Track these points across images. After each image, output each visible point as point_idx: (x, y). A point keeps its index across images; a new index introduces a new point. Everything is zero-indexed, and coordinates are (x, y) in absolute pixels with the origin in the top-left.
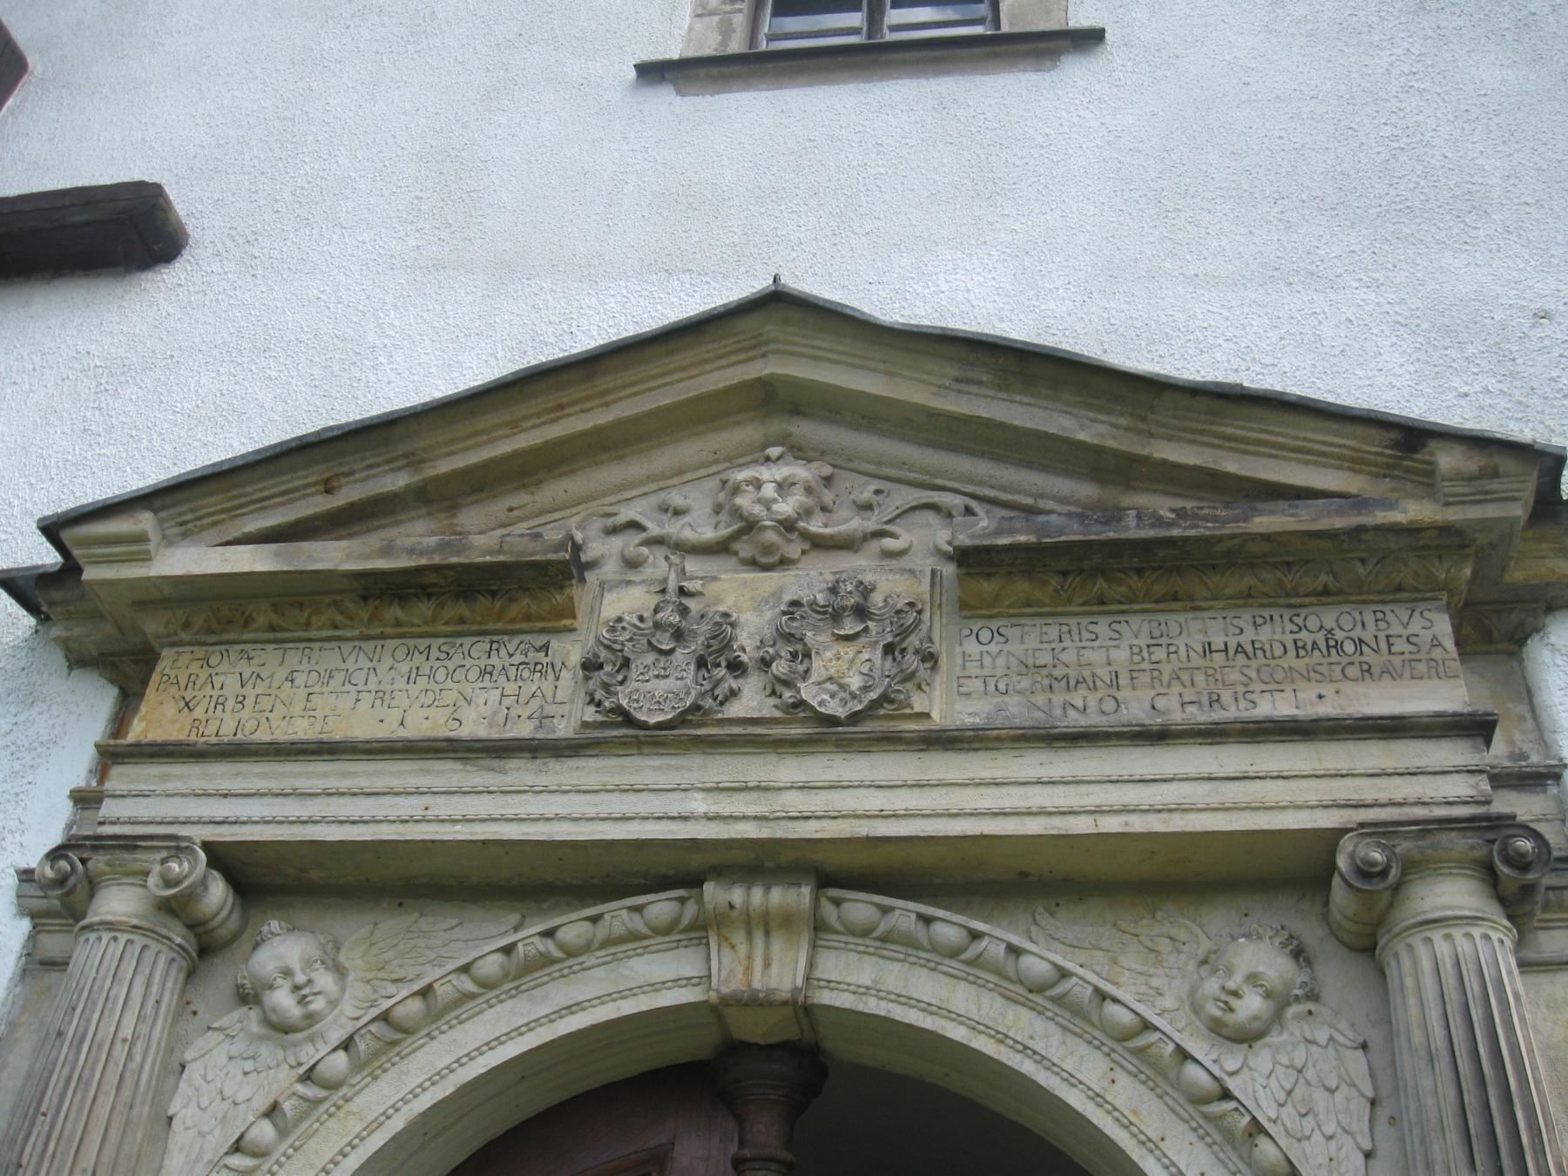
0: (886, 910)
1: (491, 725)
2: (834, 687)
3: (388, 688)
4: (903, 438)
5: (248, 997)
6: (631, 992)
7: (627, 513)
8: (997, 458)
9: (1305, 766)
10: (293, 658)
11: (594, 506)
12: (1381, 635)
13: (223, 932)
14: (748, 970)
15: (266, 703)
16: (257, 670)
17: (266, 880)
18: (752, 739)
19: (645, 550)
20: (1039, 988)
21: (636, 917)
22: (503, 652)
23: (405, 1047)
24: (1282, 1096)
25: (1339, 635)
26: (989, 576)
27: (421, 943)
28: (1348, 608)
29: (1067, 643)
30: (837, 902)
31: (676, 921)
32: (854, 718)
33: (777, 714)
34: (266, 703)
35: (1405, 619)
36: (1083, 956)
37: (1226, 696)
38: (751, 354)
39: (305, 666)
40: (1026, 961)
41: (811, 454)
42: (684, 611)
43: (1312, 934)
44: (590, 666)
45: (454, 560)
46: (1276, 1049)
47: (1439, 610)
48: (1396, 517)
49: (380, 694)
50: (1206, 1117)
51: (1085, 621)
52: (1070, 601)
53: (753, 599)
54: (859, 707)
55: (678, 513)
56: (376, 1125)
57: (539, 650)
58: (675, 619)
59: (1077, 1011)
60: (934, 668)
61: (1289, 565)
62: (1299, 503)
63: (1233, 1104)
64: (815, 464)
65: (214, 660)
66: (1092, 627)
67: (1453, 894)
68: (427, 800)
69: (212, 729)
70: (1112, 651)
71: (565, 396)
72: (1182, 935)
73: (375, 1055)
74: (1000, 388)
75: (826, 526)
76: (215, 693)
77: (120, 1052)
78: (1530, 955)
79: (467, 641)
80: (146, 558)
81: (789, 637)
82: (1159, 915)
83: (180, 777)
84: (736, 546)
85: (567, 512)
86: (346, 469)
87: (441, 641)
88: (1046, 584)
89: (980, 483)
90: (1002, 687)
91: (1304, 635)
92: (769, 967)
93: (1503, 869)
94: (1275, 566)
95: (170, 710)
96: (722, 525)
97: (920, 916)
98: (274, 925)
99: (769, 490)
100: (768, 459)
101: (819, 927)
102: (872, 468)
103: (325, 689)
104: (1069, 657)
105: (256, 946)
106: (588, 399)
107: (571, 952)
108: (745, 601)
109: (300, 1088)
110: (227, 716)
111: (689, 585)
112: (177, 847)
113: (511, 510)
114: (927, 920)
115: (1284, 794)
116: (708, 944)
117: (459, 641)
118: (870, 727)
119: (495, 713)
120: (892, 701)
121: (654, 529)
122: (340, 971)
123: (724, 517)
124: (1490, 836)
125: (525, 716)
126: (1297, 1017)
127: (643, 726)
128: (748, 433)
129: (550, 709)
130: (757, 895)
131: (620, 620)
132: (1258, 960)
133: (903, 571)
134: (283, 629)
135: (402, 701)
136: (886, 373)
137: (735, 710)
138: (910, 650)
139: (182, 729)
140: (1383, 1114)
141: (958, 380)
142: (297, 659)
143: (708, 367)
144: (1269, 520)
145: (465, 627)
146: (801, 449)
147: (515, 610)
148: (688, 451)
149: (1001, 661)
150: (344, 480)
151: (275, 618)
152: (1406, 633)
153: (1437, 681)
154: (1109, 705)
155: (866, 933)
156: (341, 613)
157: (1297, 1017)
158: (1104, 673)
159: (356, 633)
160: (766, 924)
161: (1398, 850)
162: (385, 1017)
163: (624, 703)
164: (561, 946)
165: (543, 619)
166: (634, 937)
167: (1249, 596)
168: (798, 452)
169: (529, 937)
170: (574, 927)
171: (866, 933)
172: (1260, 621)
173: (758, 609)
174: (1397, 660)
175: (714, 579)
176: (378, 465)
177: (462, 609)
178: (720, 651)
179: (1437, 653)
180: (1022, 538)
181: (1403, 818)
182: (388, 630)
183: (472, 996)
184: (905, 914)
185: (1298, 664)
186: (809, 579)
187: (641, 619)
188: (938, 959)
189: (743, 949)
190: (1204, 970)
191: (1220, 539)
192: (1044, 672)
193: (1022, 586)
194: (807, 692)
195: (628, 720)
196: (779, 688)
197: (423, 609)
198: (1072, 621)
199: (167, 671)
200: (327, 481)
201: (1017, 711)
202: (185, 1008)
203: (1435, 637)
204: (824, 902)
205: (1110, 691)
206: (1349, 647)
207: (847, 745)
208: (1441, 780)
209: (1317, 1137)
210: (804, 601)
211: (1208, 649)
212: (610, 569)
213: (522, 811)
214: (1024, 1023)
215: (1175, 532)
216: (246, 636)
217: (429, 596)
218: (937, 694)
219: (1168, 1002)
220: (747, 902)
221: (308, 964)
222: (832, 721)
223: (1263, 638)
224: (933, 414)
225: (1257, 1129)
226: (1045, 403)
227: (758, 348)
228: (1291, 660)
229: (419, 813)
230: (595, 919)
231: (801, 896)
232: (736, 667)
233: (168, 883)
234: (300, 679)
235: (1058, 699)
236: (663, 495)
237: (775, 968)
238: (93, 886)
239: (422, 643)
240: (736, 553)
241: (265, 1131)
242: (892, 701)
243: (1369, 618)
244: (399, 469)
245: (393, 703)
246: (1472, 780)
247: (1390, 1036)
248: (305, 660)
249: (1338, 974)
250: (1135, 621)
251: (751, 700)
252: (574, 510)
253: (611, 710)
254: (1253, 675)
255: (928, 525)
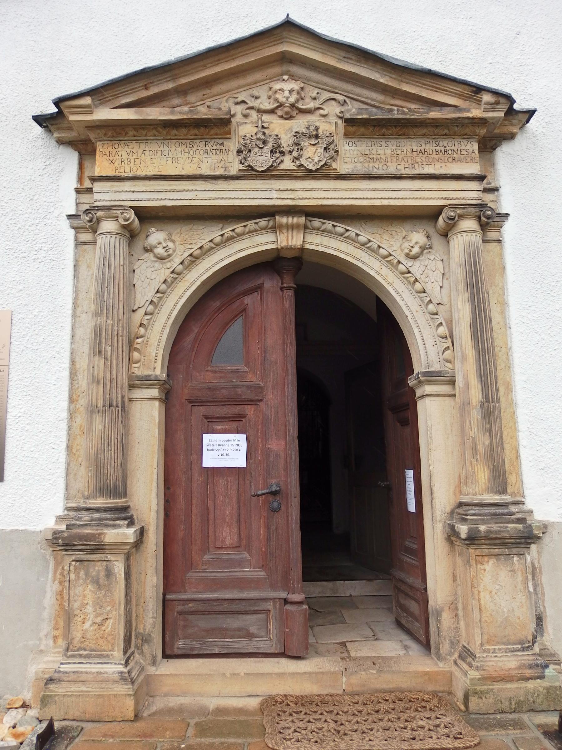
0: (323, 223)
1: (211, 170)
2: (310, 160)
3: (176, 157)
4: (325, 75)
5: (148, 250)
6: (256, 246)
7: (241, 98)
8: (354, 84)
9: (435, 187)
10: (143, 146)
11: (229, 94)
12: (459, 149)
13: (137, 232)
14: (287, 240)
15: (137, 161)
16: (132, 150)
17: (148, 216)
18: (288, 176)
19: (248, 111)
20: (364, 244)
21: (256, 225)
22: (210, 145)
23: (197, 262)
24: (422, 273)
25: (448, 148)
26: (352, 126)
27: (195, 233)
28: (451, 140)
29: (373, 147)
30: (310, 221)
31: (267, 226)
32: (317, 170)
33: (295, 168)
34: (137, 161)
35: (466, 144)
36: (373, 236)
37: (416, 165)
38: (278, 42)
39: (147, 149)
40: (360, 238)
41: (296, 78)
42: (264, 134)
43: (431, 231)
44: (239, 152)
45: (195, 117)
46: (421, 260)
47: (475, 141)
48: (470, 115)
49: (174, 159)
50: (404, 277)
51: (378, 140)
52: (375, 135)
53: (284, 130)
54: (319, 167)
55: (257, 98)
56: (192, 284)
57: (221, 145)
58: (263, 137)
59: (373, 251)
60: (337, 155)
61: (437, 126)
62: (443, 108)
63: (411, 275)
64: (298, 82)
65: (116, 146)
66: (380, 143)
67: (470, 224)
68: (196, 193)
69: (122, 170)
70: (386, 150)
71: (221, 56)
72: (399, 231)
73: (189, 265)
74: (357, 61)
75: (303, 105)
76: (120, 158)
77: (121, 268)
78: (485, 239)
79: (198, 141)
80: (91, 113)
81: (297, 144)
82: (393, 225)
83: (117, 186)
84: (277, 111)
85: (221, 96)
86: (151, 81)
87: (190, 141)
88: (369, 129)
89: (348, 92)
90: (356, 161)
91: (438, 148)
92: (292, 240)
93: (483, 219)
94: (433, 126)
95: (106, 163)
96: (271, 103)
97: (333, 225)
98: (153, 229)
99: (287, 93)
100: (284, 80)
101: (306, 227)
102: (315, 84)
103: (156, 157)
104: (374, 152)
105: (147, 236)
106: (228, 57)
107: (239, 235)
108: (282, 130)
109: (172, 275)
110: (126, 166)
111: (265, 125)
112: (124, 209)
113: (204, 95)
114: (334, 226)
115: (428, 195)
116: (276, 232)
117: (195, 141)
118: (322, 173)
119: (211, 166)
120: (327, 165)
121: (251, 104)
122: (173, 241)
123: (272, 100)
124: (481, 209)
125: (220, 167)
126: (427, 253)
127: (258, 171)
128: (276, 70)
129: (228, 165)
130: (290, 220)
131: (245, 136)
132: (417, 237)
133: (327, 122)
134: (138, 137)
135: (181, 161)
136: (322, 53)
137: (282, 166)
138: (331, 149)
139: (112, 170)
140: (445, 277)
141: (344, 57)
142: (144, 147)
143: (265, 46)
144: (435, 114)
145: (197, 137)
146: (293, 76)
147: (212, 132)
148: (258, 76)
149: (355, 152)
150: (151, 85)
151: (135, 133)
152: (466, 148)
153: (472, 164)
154: (385, 167)
155: (318, 229)
156: (157, 131)
157: (427, 253)
158: (383, 157)
159: (162, 138)
160: (292, 227)
161: (458, 212)
162: (191, 255)
163: (251, 164)
164: (236, 234)
165: (221, 135)
166: (256, 231)
167: (425, 135)
168: (293, 77)
169: (227, 231)
170: (239, 228)
171: (318, 229)
172: (426, 142)
173: (286, 134)
174: (462, 156)
175: (272, 122)
176: (162, 80)
177: (196, 131)
178: (277, 148)
179: (473, 155)
180: (365, 116)
181: (460, 203)
182: (172, 137)
183: (214, 248)
184: (329, 225)
185: (436, 157)
186: (300, 123)
187: (252, 136)
188: (337, 236)
189: (286, 234)
190: (404, 240)
191: (419, 119)
192: (367, 156)
193: (362, 130)
194: (303, 161)
195: (251, 168)
196: (295, 160)
197: (184, 131)
198: (375, 140)
199: (101, 150)
200: (145, 85)
201: (360, 169)
202: (130, 254)
203: (473, 150)
204: (307, 221)
205: (386, 163)
206: (450, 152)
207: (314, 178)
208: (469, 193)
209: (429, 282)
210: (300, 132)
211: (412, 151)
212: (239, 118)
213: (225, 196)
214: (359, 253)
215: (408, 116)
216: (125, 138)
217: (185, 127)
218: (338, 162)
219: (395, 248)
220: (288, 222)
221: (165, 240)
222: (311, 171)
223: (427, 148)
224: (336, 68)
225: (416, 280)
226: (370, 68)
227: (281, 41)
228: (434, 156)
229: (194, 197)
230: (245, 226)
231: (302, 220)
232: (282, 153)
233: (126, 220)
234: (147, 153)
235: (371, 165)
236: (251, 90)
237: (294, 239)
238: (99, 221)
239: (184, 141)
240: (277, 113)
241: (164, 287)
242: (327, 165)
243: (456, 143)
244: (169, 81)
245: (179, 162)
246: (478, 193)
247: (449, 258)
248: (147, 147)
249: (437, 242)
250: (392, 141)
251: (288, 163)
252: (224, 95)
253: (247, 166)
254: (424, 159)
255: (333, 106)
